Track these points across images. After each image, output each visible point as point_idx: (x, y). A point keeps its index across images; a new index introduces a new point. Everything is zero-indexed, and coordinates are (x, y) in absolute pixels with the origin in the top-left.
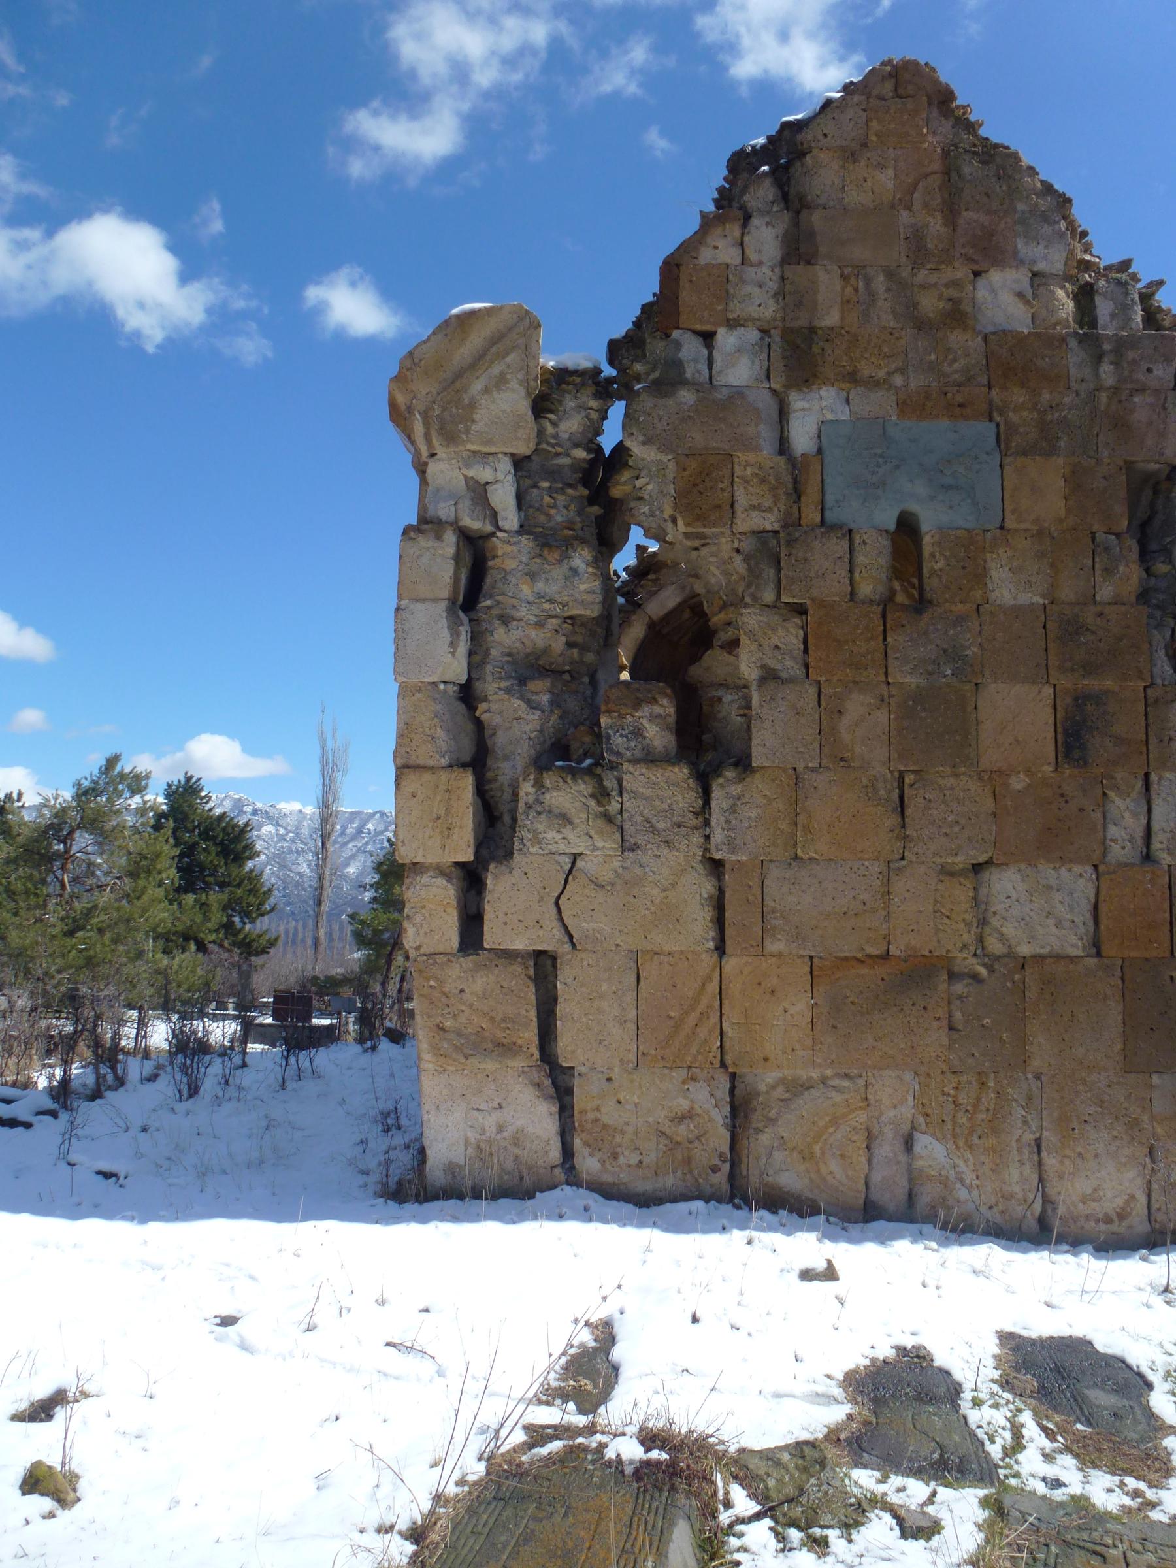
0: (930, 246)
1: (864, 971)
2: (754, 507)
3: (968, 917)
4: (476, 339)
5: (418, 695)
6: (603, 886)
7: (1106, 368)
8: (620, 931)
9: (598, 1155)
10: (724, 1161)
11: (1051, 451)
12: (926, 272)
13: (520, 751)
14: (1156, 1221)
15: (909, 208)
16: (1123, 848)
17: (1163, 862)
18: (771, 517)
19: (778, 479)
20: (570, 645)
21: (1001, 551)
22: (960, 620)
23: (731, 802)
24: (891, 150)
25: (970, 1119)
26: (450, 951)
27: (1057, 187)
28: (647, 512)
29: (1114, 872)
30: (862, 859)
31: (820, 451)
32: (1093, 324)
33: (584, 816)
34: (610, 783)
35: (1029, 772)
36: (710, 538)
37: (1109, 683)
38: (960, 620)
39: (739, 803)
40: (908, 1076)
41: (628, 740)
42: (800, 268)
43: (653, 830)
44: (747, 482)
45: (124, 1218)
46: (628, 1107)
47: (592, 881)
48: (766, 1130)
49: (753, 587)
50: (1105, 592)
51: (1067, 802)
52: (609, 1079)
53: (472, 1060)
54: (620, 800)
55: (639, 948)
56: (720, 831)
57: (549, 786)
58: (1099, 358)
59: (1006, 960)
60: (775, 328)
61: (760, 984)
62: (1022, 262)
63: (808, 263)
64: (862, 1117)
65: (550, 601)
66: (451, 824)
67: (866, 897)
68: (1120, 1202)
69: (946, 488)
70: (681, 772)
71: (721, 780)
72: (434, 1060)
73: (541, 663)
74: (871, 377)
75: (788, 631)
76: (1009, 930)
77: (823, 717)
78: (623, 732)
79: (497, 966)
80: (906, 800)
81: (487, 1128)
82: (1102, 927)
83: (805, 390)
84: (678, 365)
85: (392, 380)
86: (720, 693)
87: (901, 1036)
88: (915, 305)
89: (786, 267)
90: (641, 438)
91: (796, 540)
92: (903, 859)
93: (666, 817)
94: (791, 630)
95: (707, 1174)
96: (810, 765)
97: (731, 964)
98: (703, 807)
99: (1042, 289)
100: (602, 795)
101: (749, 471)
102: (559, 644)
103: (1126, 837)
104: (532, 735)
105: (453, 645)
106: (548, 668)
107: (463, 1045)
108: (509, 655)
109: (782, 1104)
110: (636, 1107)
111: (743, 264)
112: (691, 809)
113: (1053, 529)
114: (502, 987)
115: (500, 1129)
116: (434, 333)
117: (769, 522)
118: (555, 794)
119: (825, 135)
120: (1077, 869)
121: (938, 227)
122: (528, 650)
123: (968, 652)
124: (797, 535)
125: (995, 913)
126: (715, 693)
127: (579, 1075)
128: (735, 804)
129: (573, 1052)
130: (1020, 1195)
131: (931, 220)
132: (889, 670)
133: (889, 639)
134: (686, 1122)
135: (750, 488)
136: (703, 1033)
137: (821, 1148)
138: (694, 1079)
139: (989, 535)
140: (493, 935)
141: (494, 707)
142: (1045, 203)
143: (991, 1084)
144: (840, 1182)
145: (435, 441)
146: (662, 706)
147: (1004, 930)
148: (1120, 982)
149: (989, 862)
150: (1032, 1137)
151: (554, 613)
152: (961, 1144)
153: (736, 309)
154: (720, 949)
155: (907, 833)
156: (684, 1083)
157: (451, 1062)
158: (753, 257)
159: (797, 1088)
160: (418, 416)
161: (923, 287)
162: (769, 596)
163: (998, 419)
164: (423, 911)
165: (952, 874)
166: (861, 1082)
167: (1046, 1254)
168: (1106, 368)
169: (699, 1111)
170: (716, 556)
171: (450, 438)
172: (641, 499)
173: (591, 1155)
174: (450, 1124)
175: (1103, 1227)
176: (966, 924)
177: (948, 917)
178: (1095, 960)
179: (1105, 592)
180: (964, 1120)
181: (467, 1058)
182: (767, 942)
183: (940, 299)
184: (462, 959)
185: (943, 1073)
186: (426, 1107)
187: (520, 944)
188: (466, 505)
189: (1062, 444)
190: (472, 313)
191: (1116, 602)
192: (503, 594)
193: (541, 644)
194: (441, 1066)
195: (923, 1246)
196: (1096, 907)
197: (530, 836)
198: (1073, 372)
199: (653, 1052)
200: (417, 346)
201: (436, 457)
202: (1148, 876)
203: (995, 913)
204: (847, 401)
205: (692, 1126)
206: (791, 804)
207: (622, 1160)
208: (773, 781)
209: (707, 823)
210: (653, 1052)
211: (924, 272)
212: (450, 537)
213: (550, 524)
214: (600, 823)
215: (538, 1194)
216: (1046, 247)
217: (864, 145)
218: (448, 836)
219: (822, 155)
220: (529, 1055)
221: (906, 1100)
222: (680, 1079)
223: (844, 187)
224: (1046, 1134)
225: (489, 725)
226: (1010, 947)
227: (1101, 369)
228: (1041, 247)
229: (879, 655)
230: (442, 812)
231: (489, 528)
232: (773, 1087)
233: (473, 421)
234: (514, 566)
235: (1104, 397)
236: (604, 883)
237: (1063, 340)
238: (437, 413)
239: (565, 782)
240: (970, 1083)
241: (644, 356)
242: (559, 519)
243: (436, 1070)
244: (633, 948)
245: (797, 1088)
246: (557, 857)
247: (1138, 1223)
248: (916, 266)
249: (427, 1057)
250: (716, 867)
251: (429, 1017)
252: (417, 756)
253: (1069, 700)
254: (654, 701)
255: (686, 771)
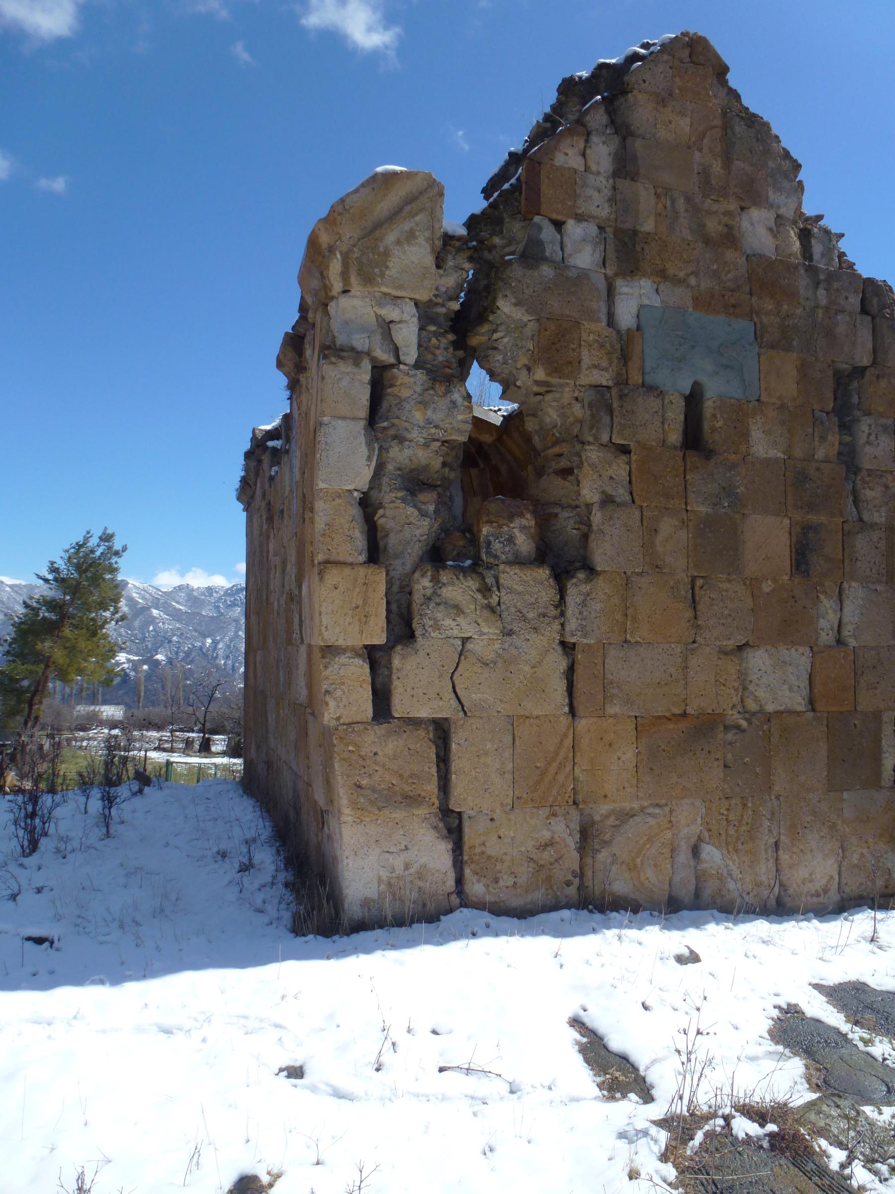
0: (713, 182)
1: (671, 726)
2: (595, 366)
3: (736, 684)
4: (394, 197)
5: (338, 501)
6: (487, 664)
7: (821, 292)
8: (501, 701)
9: (484, 880)
10: (575, 877)
11: (788, 349)
12: (711, 201)
13: (409, 551)
14: (844, 892)
15: (700, 150)
16: (828, 635)
17: (850, 644)
18: (607, 376)
19: (612, 346)
20: (444, 464)
21: (758, 417)
22: (734, 466)
23: (582, 597)
24: (688, 103)
25: (736, 831)
26: (365, 720)
27: (792, 154)
28: (501, 361)
29: (823, 652)
30: (669, 643)
31: (639, 328)
32: (811, 259)
33: (472, 607)
34: (490, 580)
35: (774, 580)
36: (555, 386)
37: (823, 518)
38: (734, 466)
39: (588, 599)
40: (698, 803)
41: (504, 546)
42: (627, 182)
43: (525, 619)
44: (590, 345)
45: (94, 982)
46: (506, 840)
47: (478, 660)
48: (603, 850)
49: (595, 429)
50: (820, 454)
51: (796, 602)
52: (492, 820)
53: (386, 812)
54: (499, 594)
55: (515, 713)
56: (575, 620)
57: (445, 582)
58: (817, 284)
59: (759, 715)
60: (610, 227)
61: (602, 739)
62: (771, 206)
63: (632, 179)
64: (669, 835)
65: (436, 427)
66: (368, 612)
67: (672, 670)
68: (824, 881)
69: (727, 367)
70: (543, 573)
71: (575, 580)
72: (352, 813)
73: (421, 477)
74: (675, 276)
75: (619, 466)
76: (761, 693)
77: (645, 534)
78: (501, 539)
79: (405, 732)
80: (697, 598)
81: (396, 867)
82: (816, 691)
83: (629, 278)
84: (540, 244)
85: (320, 221)
86: (556, 511)
87: (694, 773)
88: (704, 225)
89: (618, 180)
90: (513, 300)
91: (626, 395)
92: (694, 642)
93: (534, 608)
94: (621, 465)
95: (563, 888)
96: (637, 570)
97: (582, 724)
98: (560, 601)
99: (782, 229)
100: (485, 590)
101: (591, 337)
102: (437, 463)
103: (829, 627)
104: (423, 538)
105: (369, 458)
106: (425, 481)
107: (376, 799)
108: (399, 469)
109: (614, 829)
110: (512, 840)
111: (585, 171)
112: (552, 602)
113: (789, 404)
114: (409, 749)
115: (407, 867)
116: (363, 185)
117: (604, 378)
118: (450, 588)
119: (644, 81)
120: (801, 649)
121: (718, 169)
122: (413, 467)
123: (738, 491)
124: (626, 391)
125: (751, 682)
126: (552, 510)
127: (469, 817)
128: (586, 599)
129: (465, 799)
130: (766, 883)
131: (714, 162)
132: (689, 501)
133: (688, 477)
134: (549, 849)
135: (592, 351)
136: (561, 778)
137: (641, 860)
138: (555, 815)
139: (751, 405)
140: (400, 706)
141: (389, 513)
142: (786, 165)
143: (750, 805)
144: (653, 885)
145: (354, 280)
146: (527, 519)
147: (757, 694)
148: (826, 729)
149: (747, 644)
150: (774, 840)
151: (437, 437)
152: (731, 850)
153: (583, 207)
154: (572, 711)
155: (699, 623)
156: (547, 818)
157: (367, 814)
158: (594, 167)
159: (625, 816)
160: (338, 256)
161: (709, 212)
162: (605, 438)
163: (756, 319)
164: (343, 687)
165: (726, 653)
166: (667, 809)
167: (793, 923)
168: (821, 292)
169: (558, 839)
170: (558, 402)
171: (368, 279)
172: (496, 348)
173: (478, 881)
174: (365, 866)
175: (815, 899)
176: (735, 690)
177: (724, 685)
178: (812, 714)
179: (820, 454)
180: (733, 832)
181: (380, 809)
182: (607, 706)
183: (719, 223)
184: (376, 727)
185: (720, 799)
186: (346, 854)
187: (424, 713)
188: (377, 338)
189: (795, 343)
190: (395, 174)
191: (826, 461)
192: (397, 418)
193: (424, 462)
194: (359, 818)
195: (723, 927)
196: (810, 675)
197: (431, 623)
198: (802, 291)
199: (525, 796)
200: (348, 195)
201: (350, 294)
202: (842, 654)
203: (751, 682)
204: (657, 291)
205: (552, 851)
206: (623, 600)
207: (501, 883)
208: (611, 582)
209: (562, 614)
210: (525, 796)
211: (708, 201)
212: (367, 366)
213: (435, 363)
214: (486, 613)
215: (442, 918)
216: (787, 197)
217: (671, 95)
218: (366, 623)
219: (640, 96)
220: (430, 804)
221: (696, 820)
222: (545, 816)
223: (656, 125)
224: (782, 837)
225: (383, 529)
226: (761, 706)
227: (818, 293)
228: (783, 197)
229: (681, 489)
230: (360, 602)
231: (392, 360)
232: (607, 817)
233: (387, 267)
234: (408, 395)
235: (820, 313)
236: (488, 662)
237: (796, 267)
238: (356, 255)
239: (458, 578)
240: (736, 805)
241: (502, 233)
242: (441, 358)
243: (354, 822)
244: (511, 714)
245: (625, 816)
246: (452, 641)
247: (834, 897)
248: (705, 196)
249: (346, 811)
250: (568, 648)
251: (348, 776)
252: (338, 554)
253: (799, 529)
254: (521, 515)
255: (547, 572)
